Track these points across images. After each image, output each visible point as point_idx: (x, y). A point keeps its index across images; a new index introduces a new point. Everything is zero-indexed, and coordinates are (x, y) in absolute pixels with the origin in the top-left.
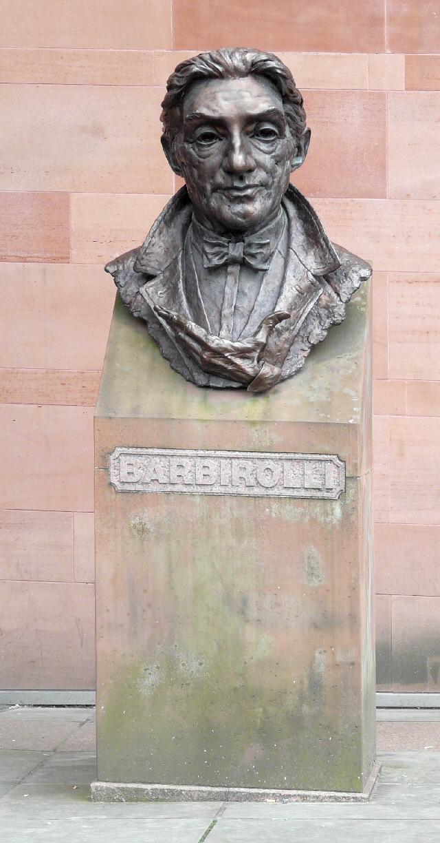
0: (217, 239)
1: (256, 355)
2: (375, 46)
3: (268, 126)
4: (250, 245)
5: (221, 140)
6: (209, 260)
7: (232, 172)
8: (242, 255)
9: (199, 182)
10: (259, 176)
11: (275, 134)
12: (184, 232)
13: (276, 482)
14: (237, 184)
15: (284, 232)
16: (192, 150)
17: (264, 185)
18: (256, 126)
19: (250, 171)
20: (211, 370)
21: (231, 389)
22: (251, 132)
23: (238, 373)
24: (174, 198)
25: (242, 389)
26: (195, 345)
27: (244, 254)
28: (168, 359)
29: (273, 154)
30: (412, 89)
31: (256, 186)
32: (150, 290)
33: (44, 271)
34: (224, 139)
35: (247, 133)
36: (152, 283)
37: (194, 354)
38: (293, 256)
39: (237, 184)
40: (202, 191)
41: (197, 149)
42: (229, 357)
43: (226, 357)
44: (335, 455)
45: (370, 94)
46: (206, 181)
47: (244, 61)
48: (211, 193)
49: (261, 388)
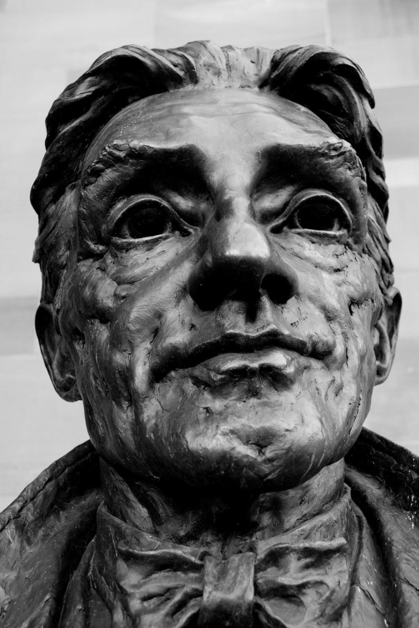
4: (275, 558)
5: (185, 234)
8: (250, 596)
24: (56, 470)
27: (257, 592)
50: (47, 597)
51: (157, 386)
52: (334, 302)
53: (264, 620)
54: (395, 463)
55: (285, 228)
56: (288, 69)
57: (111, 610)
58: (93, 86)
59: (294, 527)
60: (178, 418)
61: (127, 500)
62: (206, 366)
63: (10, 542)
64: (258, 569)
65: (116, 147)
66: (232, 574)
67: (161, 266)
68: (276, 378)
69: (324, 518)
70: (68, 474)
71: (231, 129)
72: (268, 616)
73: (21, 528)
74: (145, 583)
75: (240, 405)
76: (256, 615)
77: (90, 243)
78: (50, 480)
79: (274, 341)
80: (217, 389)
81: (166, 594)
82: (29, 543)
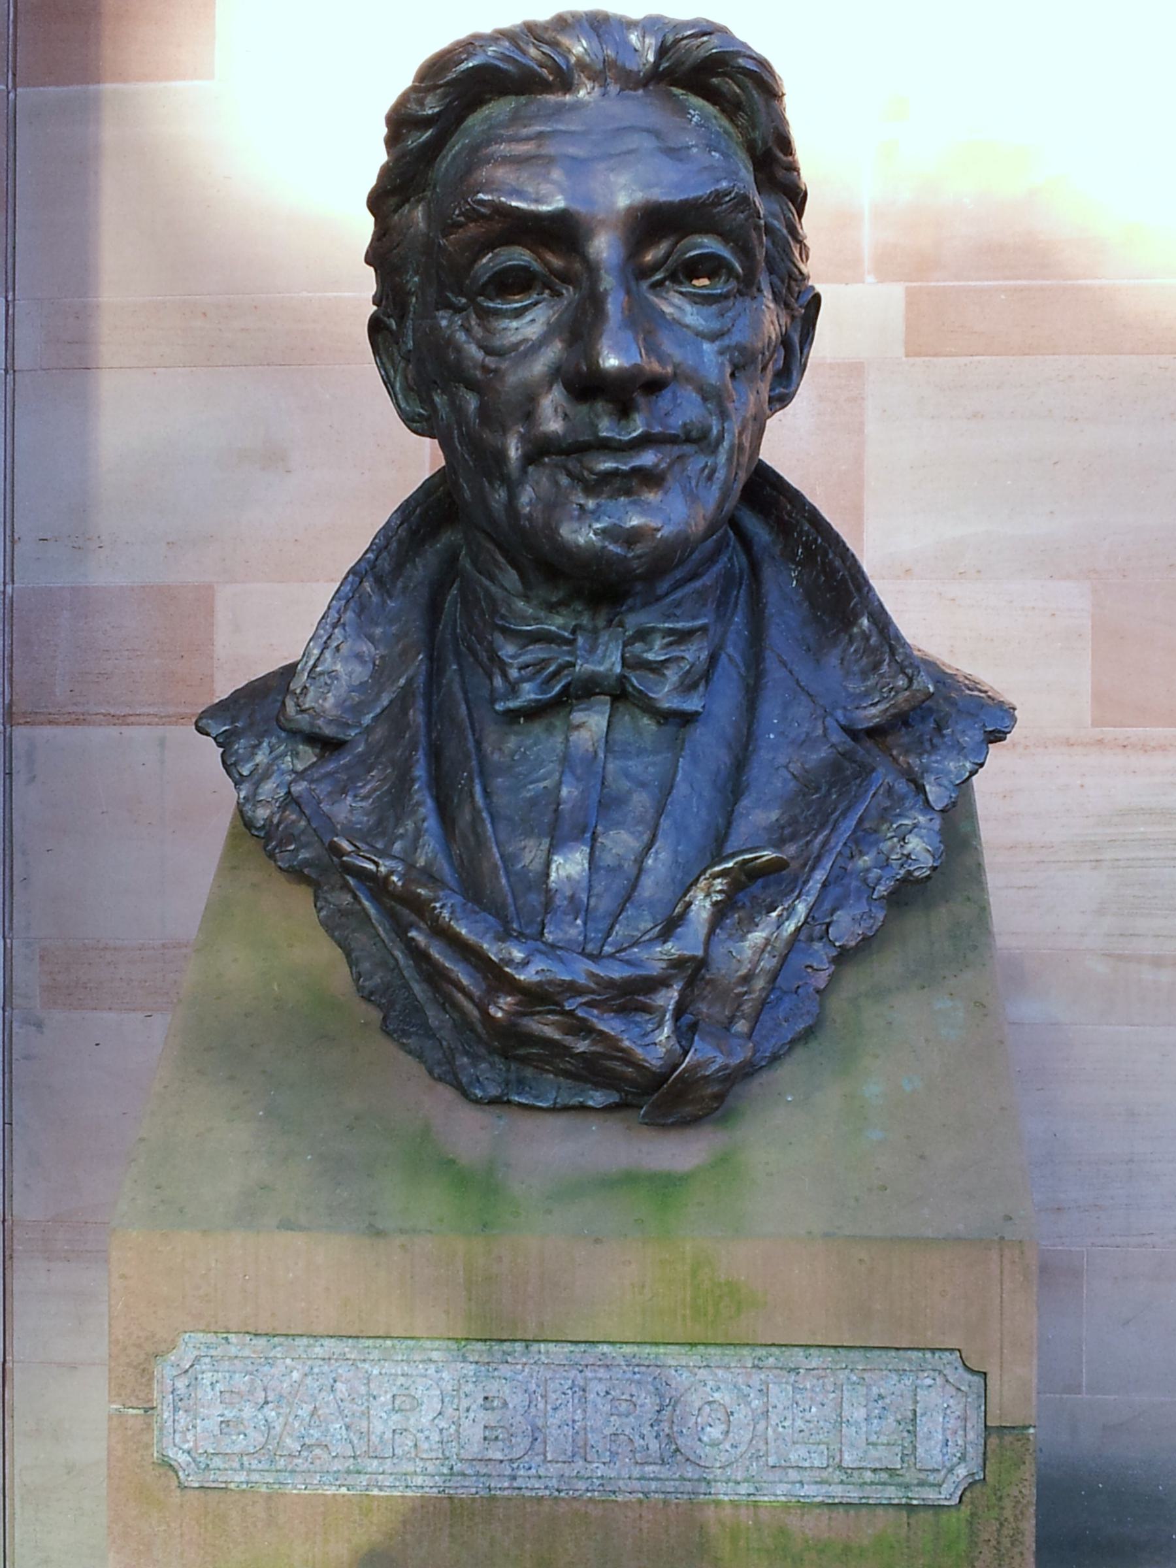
0: (537, 620)
1: (668, 998)
4: (643, 635)
5: (557, 294)
7: (587, 386)
8: (618, 669)
11: (731, 271)
12: (434, 609)
13: (742, 1448)
15: (742, 599)
16: (461, 336)
23: (609, 1064)
24: (406, 510)
26: (463, 975)
27: (624, 662)
29: (726, 341)
30: (918, 354)
31: (673, 440)
33: (162, 743)
37: (460, 996)
41: (478, 332)
42: (580, 1013)
44: (952, 1350)
46: (505, 430)
48: (524, 470)
50: (421, 656)
51: (531, 469)
53: (630, 689)
54: (789, 507)
55: (667, 283)
56: (679, 63)
57: (490, 677)
58: (446, 97)
59: (667, 594)
60: (553, 505)
61: (496, 561)
62: (581, 462)
63: (370, 596)
64: (625, 645)
65: (482, 203)
66: (601, 649)
69: (698, 584)
70: (420, 514)
72: (634, 687)
73: (379, 581)
74: (520, 655)
75: (611, 503)
76: (622, 684)
77: (449, 294)
78: (401, 524)
80: (591, 489)
81: (542, 664)
82: (390, 597)
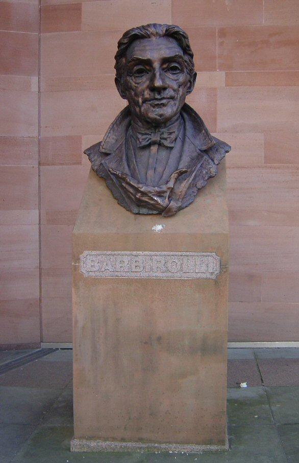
2: (213, 69)
3: (173, 65)
6: (140, 143)
7: (153, 89)
9: (136, 98)
10: (169, 93)
11: (179, 69)
12: (127, 130)
14: (158, 97)
17: (172, 98)
18: (169, 64)
19: (165, 89)
20: (140, 203)
21: (152, 214)
22: (166, 68)
24: (122, 112)
25: (159, 214)
26: (131, 190)
28: (117, 199)
32: (107, 162)
34: (149, 73)
35: (163, 69)
36: (109, 157)
38: (187, 140)
39: (158, 97)
40: (137, 104)
43: (150, 196)
45: (210, 89)
47: (154, 94)
49: (170, 214)
52: (176, 87)
67: (142, 83)
68: (164, 105)
71: (156, 51)
79: (163, 98)
